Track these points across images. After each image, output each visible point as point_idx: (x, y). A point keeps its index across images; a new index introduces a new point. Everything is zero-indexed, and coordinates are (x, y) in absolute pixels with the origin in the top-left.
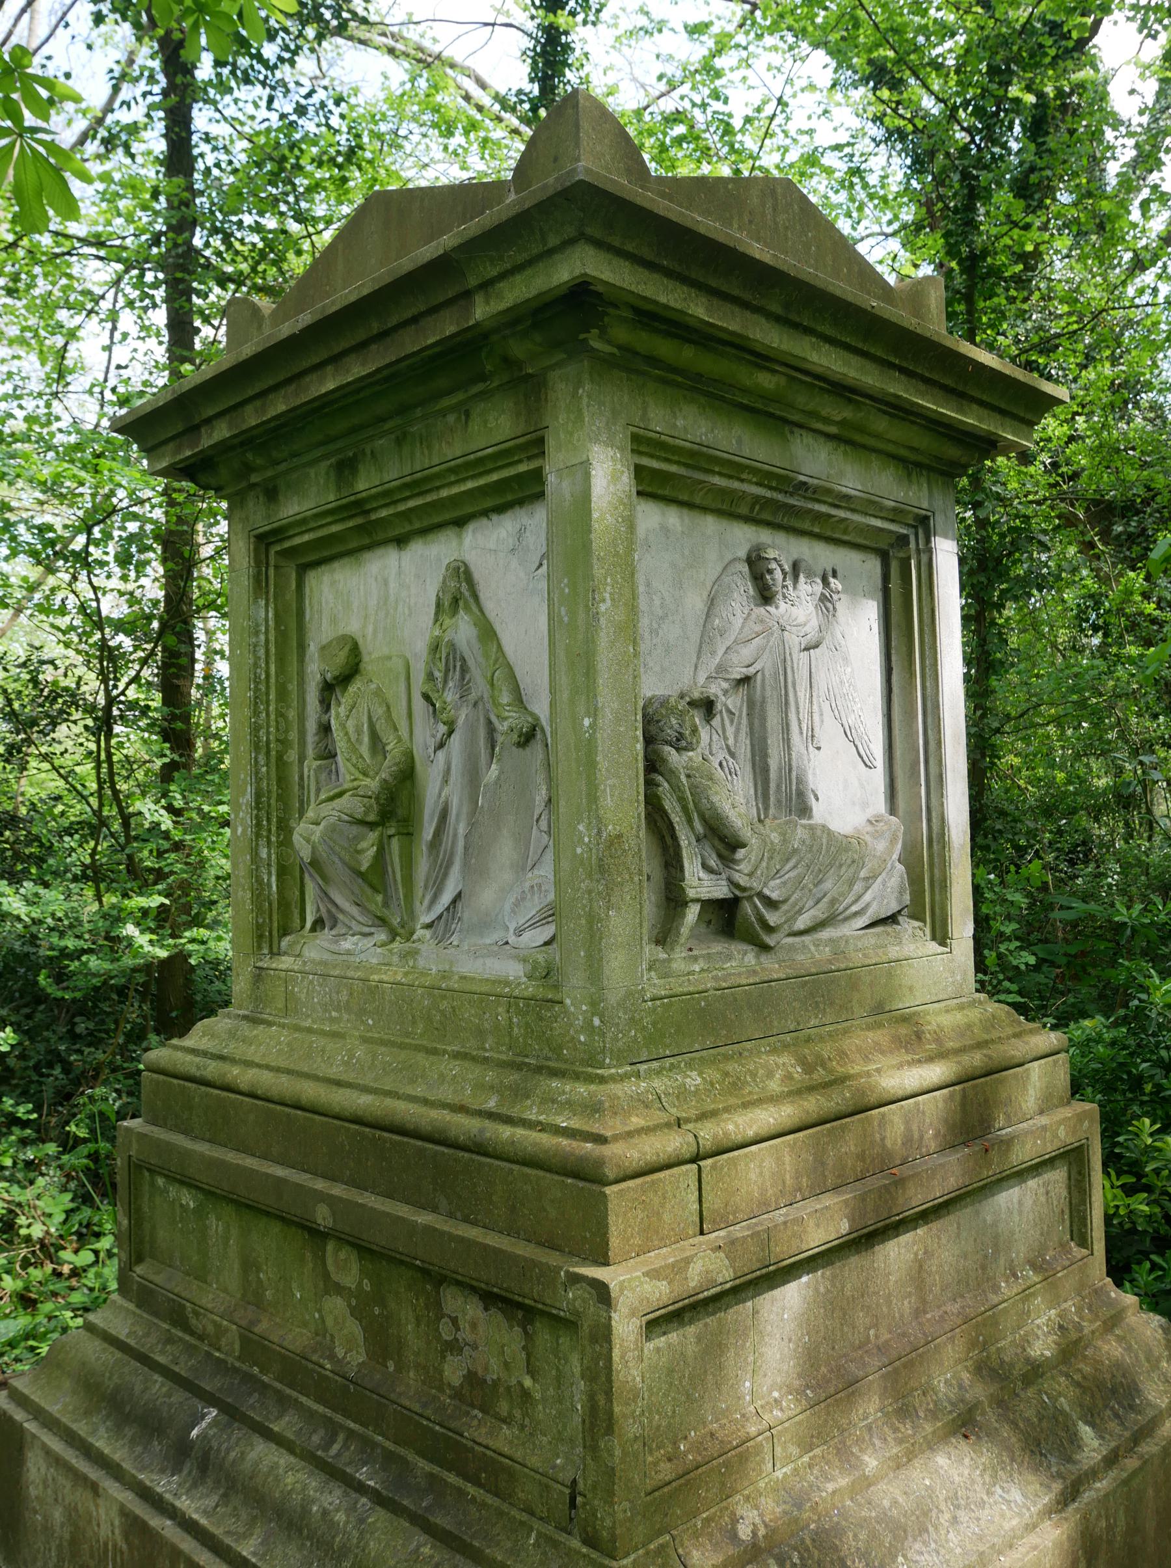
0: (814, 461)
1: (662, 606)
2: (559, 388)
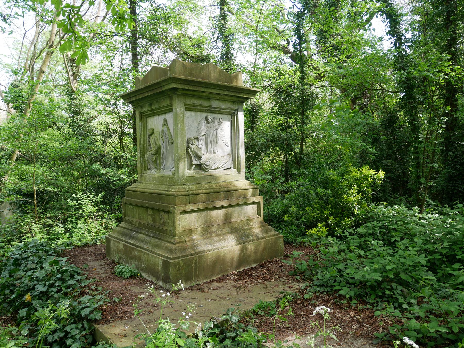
0: (215, 103)
2: (174, 98)
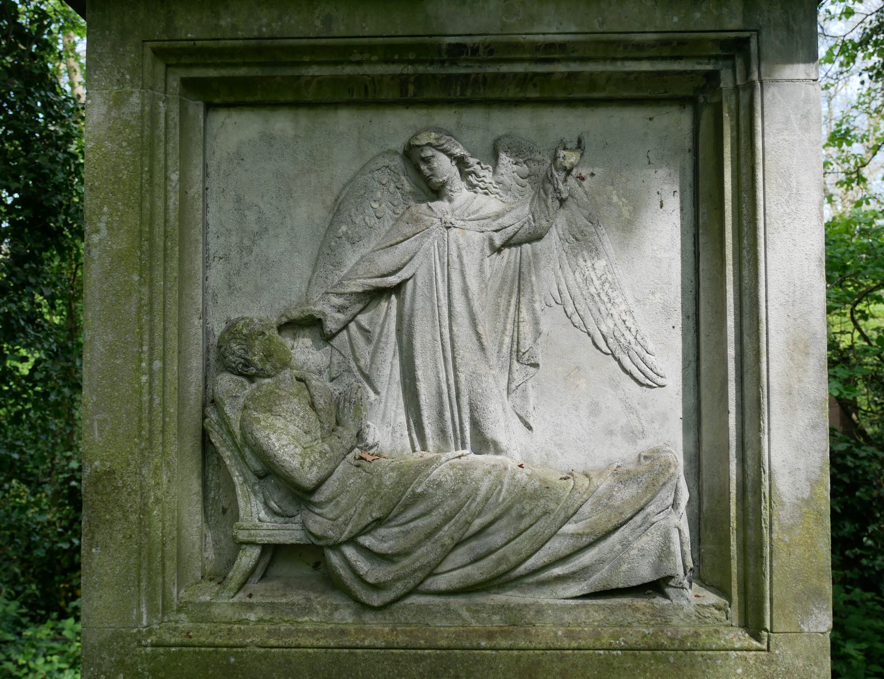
1: (259, 220)
